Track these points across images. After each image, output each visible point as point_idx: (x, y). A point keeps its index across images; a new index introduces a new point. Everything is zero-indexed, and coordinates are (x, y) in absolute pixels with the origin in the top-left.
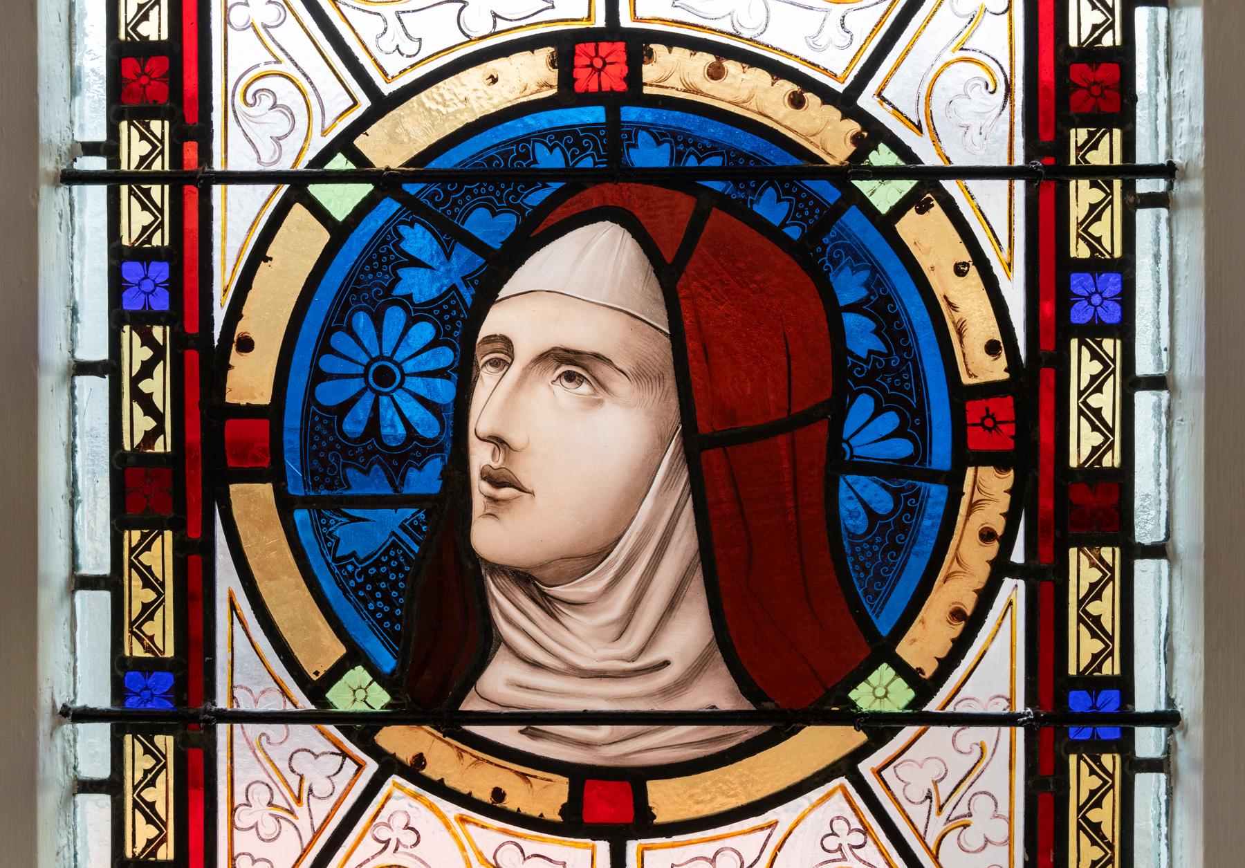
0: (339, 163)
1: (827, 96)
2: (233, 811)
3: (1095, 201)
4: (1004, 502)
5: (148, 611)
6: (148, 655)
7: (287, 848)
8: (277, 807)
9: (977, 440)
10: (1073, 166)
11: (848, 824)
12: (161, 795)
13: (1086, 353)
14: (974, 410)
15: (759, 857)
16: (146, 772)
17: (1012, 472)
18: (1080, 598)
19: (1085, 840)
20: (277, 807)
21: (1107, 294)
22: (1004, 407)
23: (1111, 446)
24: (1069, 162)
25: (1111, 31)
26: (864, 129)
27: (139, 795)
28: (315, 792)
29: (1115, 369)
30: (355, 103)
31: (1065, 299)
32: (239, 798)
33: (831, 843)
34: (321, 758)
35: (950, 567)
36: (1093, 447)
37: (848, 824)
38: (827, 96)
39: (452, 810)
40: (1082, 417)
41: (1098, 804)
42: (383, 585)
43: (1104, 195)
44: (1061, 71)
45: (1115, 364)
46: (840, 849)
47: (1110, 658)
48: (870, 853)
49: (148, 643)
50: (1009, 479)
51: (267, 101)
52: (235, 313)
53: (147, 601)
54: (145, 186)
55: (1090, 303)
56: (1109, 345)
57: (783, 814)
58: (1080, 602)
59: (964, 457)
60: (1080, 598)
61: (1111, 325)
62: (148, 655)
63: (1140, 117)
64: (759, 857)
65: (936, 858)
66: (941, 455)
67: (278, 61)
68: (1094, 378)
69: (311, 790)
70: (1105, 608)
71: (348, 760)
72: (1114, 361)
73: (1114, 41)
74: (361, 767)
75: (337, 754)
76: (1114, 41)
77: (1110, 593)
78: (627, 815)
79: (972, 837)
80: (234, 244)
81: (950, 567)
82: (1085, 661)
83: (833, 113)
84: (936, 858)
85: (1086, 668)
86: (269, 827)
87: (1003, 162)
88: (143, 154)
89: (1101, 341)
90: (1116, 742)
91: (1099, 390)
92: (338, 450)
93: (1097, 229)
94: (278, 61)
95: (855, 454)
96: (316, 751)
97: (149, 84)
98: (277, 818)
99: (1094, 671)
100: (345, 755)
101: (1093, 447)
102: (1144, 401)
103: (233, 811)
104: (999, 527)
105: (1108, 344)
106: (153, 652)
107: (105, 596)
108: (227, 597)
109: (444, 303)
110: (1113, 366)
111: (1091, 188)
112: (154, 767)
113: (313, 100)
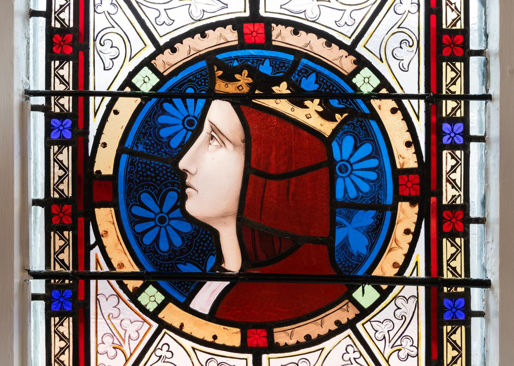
0: (128, 90)
1: (341, 45)
2: (97, 346)
4: (415, 218)
8: (115, 344)
9: (404, 191)
10: (444, 95)
13: (449, 69)
14: (403, 178)
15: (320, 11)
16: (60, 247)
20: (115, 344)
22: (416, 179)
23: (460, 108)
24: (442, 93)
25: (460, 21)
29: (461, 163)
31: (441, 134)
33: (346, 357)
36: (452, 108)
38: (341, 45)
39: (188, 344)
41: (454, 84)
42: (158, 178)
44: (439, 39)
45: (461, 249)
46: (350, 360)
47: (460, 78)
48: (361, 361)
50: (416, 209)
57: (327, 345)
59: (398, 198)
61: (459, 145)
63: (472, 116)
64: (320, 11)
65: (387, 361)
66: (389, 200)
68: (452, 79)
70: (457, 176)
72: (461, 160)
73: (461, 27)
76: (461, 27)
77: (459, 170)
78: (263, 342)
79: (402, 354)
82: (449, 111)
83: (344, 53)
84: (387, 361)
85: (450, 113)
86: (112, 352)
87: (416, 92)
89: (455, 63)
90: (462, 145)
91: (455, 171)
93: (453, 74)
99: (453, 115)
101: (452, 108)
103: (97, 346)
105: (458, 65)
110: (460, 250)
111: (451, 247)
112: (60, 355)
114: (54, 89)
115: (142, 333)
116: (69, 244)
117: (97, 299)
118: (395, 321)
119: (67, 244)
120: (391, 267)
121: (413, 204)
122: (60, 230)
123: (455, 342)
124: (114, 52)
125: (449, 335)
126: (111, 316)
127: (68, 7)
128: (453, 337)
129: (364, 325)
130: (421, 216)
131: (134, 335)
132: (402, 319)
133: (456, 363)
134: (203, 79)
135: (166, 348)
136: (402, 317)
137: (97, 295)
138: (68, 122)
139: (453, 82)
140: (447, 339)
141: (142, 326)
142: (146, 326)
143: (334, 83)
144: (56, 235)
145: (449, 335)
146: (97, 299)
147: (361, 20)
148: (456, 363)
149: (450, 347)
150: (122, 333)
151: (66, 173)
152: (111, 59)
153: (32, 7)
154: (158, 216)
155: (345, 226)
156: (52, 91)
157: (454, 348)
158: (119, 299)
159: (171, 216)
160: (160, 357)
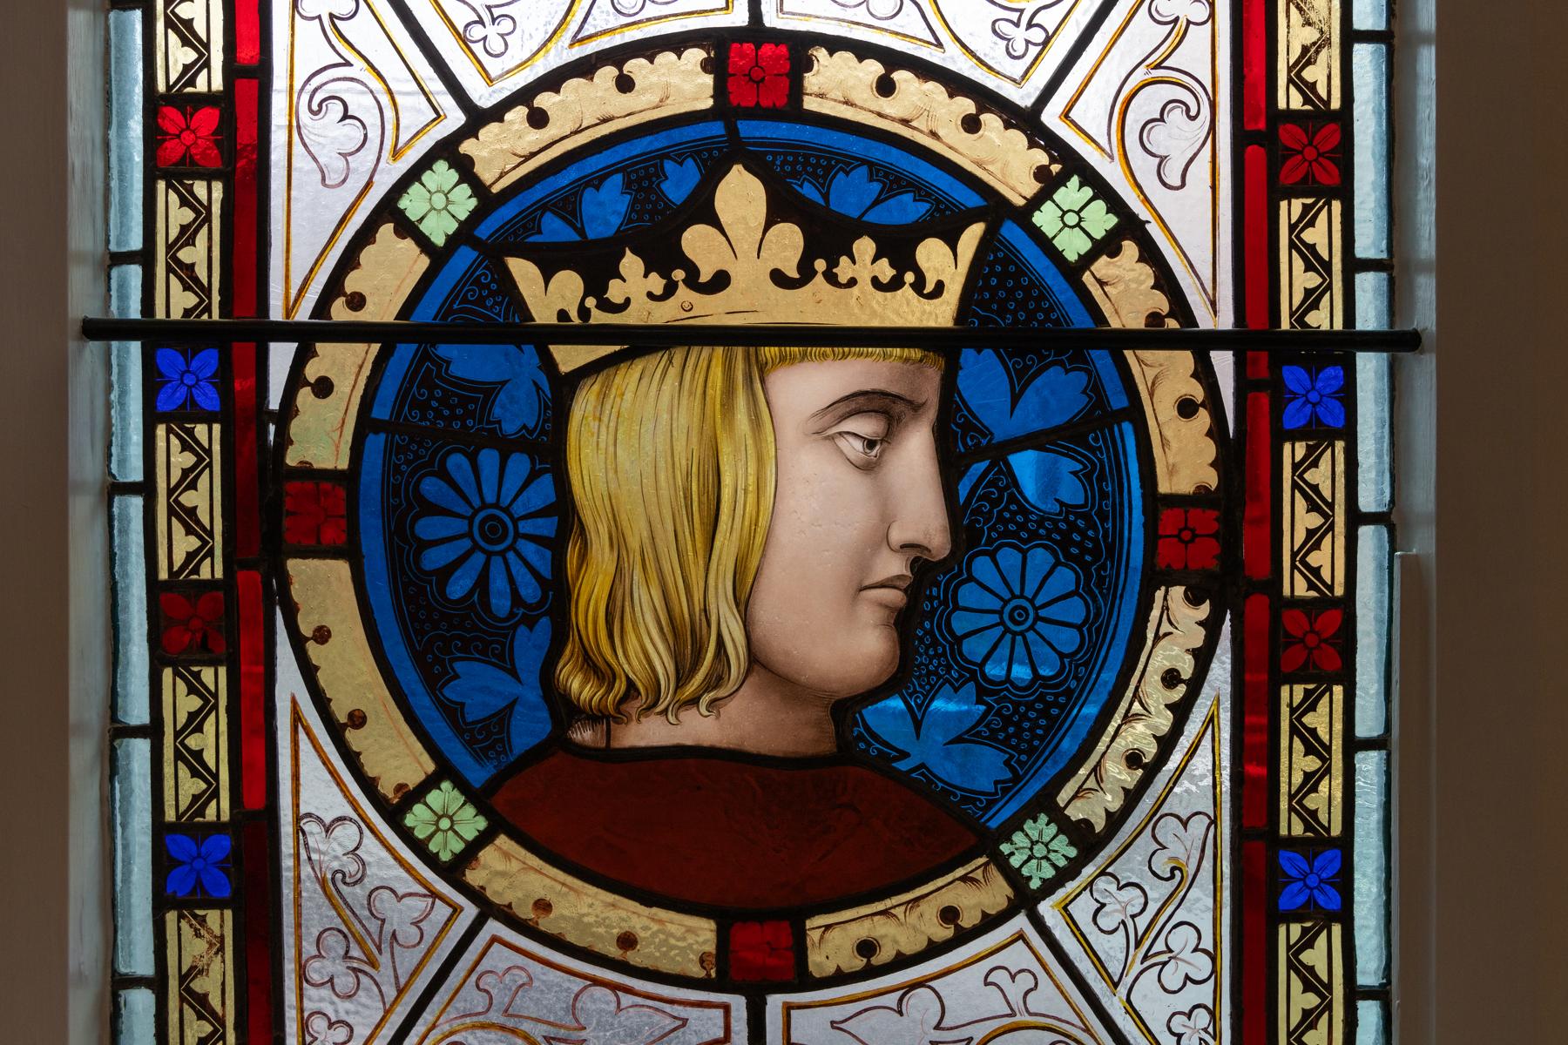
3: (1311, 285)
7: (364, 1013)
10: (1286, 332)
11: (1200, 938)
12: (211, 741)
26: (1053, 160)
27: (182, 743)
28: (400, 938)
30: (439, 116)
32: (309, 948)
34: (405, 900)
35: (894, 907)
37: (1200, 938)
51: (336, 109)
53: (191, 493)
54: (195, 669)
55: (1319, 403)
67: (348, 64)
69: (394, 935)
71: (438, 902)
74: (456, 910)
75: (425, 896)
81: (894, 907)
86: (345, 982)
88: (192, 710)
92: (480, 293)
94: (348, 64)
96: (400, 892)
97: (195, 143)
98: (355, 970)
100: (434, 895)
108: (288, 705)
113: (389, 114)
114: (168, 314)
115: (431, 929)
118: (1148, 882)
119: (209, 705)
120: (935, 911)
124: (352, 132)
127: (207, 471)
131: (409, 934)
132: (1172, 876)
135: (1019, 47)
136: (1173, 869)
137: (298, 819)
138: (208, 360)
139: (1312, 299)
141: (432, 908)
142: (442, 911)
145: (1296, 950)
147: (1132, 23)
150: (373, 926)
151: (205, 543)
152: (344, 155)
153: (113, 247)
154: (509, 541)
156: (161, 322)
158: (521, 157)
160: (1030, 25)
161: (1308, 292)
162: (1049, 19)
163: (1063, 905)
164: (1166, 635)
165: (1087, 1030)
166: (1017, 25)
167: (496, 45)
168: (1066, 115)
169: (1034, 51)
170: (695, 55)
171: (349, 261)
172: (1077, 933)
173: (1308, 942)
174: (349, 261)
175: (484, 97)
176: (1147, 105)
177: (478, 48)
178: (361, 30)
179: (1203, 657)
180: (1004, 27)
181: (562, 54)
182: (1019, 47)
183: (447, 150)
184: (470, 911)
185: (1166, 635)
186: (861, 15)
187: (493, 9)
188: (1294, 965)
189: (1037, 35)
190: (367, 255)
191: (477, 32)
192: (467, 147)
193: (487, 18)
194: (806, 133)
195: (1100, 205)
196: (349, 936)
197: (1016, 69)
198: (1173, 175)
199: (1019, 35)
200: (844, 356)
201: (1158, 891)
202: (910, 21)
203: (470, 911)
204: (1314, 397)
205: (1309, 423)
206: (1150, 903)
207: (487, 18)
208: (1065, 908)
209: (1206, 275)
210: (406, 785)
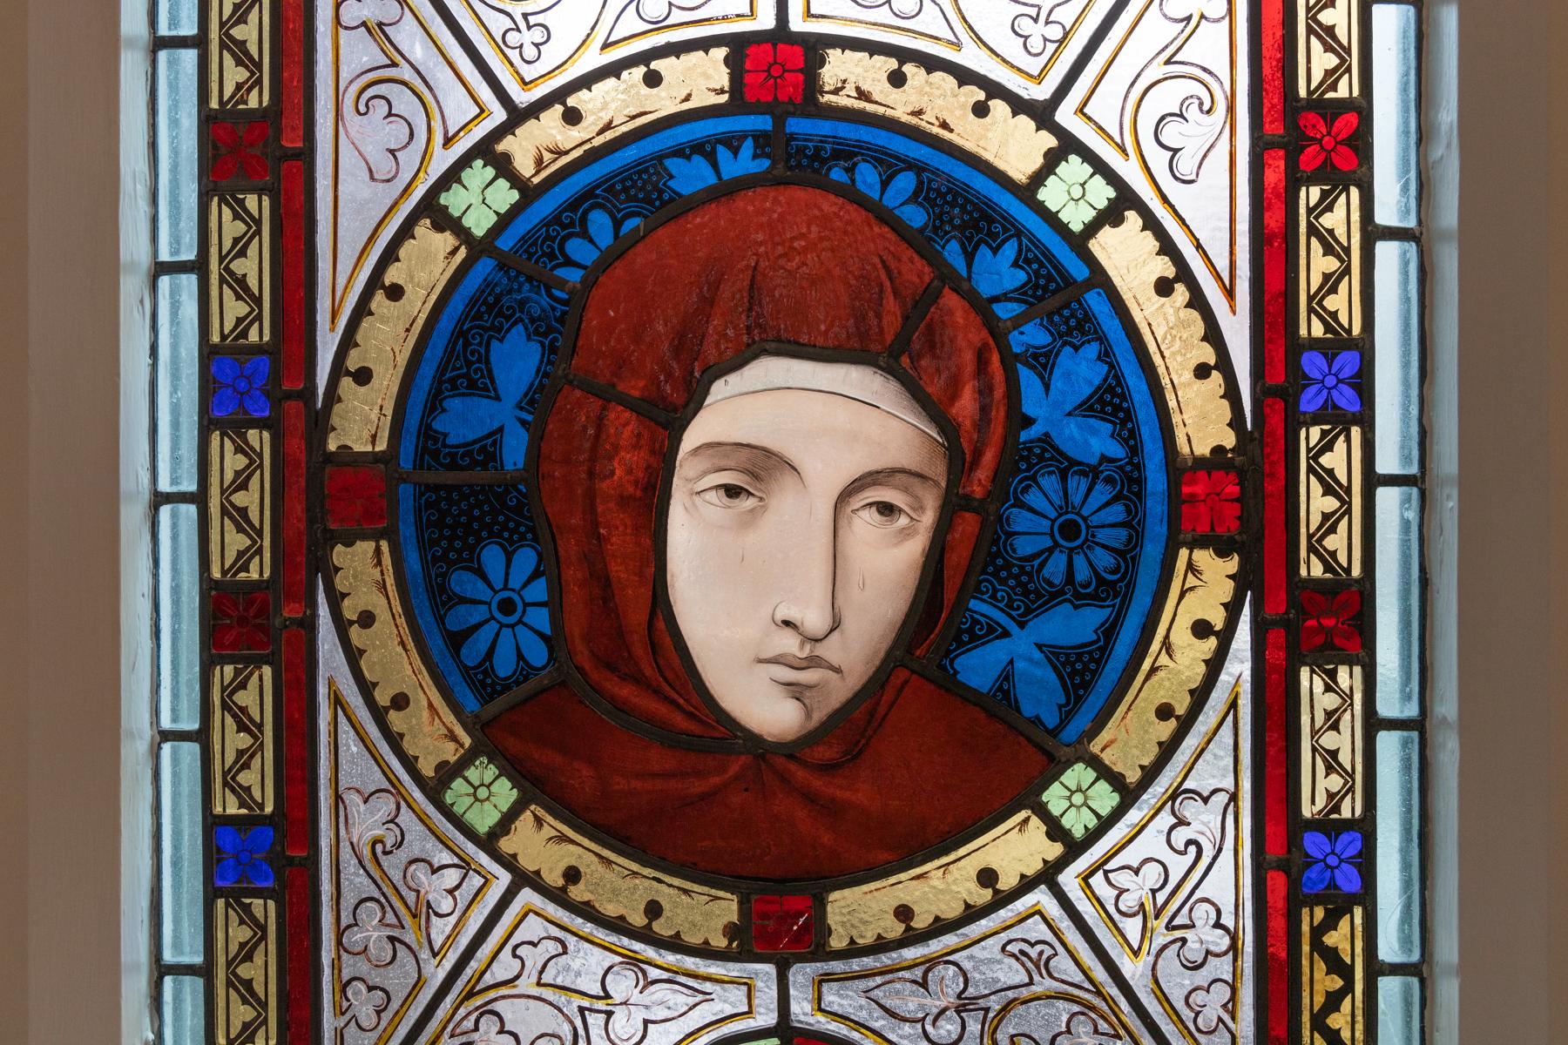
1: (1019, 105)
4: (1226, 590)
5: (244, 759)
6: (244, 811)
17: (1236, 557)
18: (1347, 277)
19: (1342, 476)
21: (1328, 850)
38: (1019, 105)
40: (1346, 245)
43: (1338, 504)
49: (243, 794)
50: (1232, 565)
51: (380, 108)
52: (348, 341)
56: (1346, 677)
58: (1347, 271)
60: (1347, 277)
62: (244, 811)
68: (1333, 530)
80: (353, 232)
95: (1056, 514)
102: (1388, 743)
104: (1218, 619)
106: (249, 808)
107: (195, 748)
109: (514, 521)
115: (464, 895)
116: (261, 466)
117: (338, 798)
121: (1222, 553)
122: (235, 428)
123: (1330, 472)
125: (1318, 932)
126: (379, 848)
128: (1326, 460)
129: (1086, 110)
130: (1241, 581)
131: (446, 905)
133: (1336, 292)
134: (536, 252)
140: (1309, 466)
143: (962, 188)
144: (227, 442)
145: (1318, 932)
146: (338, 798)
148: (1336, 292)
149: (1316, 488)
155: (1006, 634)
157: (1328, 491)
159: (499, 585)
161: (1327, 277)
162: (1066, 15)
163: (484, 115)
164: (1191, 589)
165: (1099, 993)
166: (1036, 20)
167: (530, 52)
168: (1081, 110)
169: (1051, 47)
170: (720, 53)
171: (390, 255)
172: (1111, 1003)
173: (1330, 923)
174: (390, 255)
175: (522, 98)
176: (1165, 98)
177: (514, 55)
178: (409, 39)
179: (1233, 610)
180: (1026, 26)
181: (593, 59)
182: (1036, 44)
183: (486, 150)
184: (504, 878)
185: (1191, 589)
186: (883, 15)
187: (529, 18)
188: (1317, 945)
189: (1055, 32)
190: (407, 250)
191: (513, 38)
192: (1055, 850)
193: (522, 25)
194: (825, 127)
195: (1092, 822)
196: (386, 904)
197: (1034, 66)
198: (1186, 166)
199: (1036, 31)
200: (875, 373)
201: (1178, 865)
202: (930, 21)
203: (504, 878)
204: (1330, 381)
205: (1324, 406)
206: (381, 1022)
207: (522, 25)
208: (482, 111)
209: (1222, 265)
210: (447, 762)
